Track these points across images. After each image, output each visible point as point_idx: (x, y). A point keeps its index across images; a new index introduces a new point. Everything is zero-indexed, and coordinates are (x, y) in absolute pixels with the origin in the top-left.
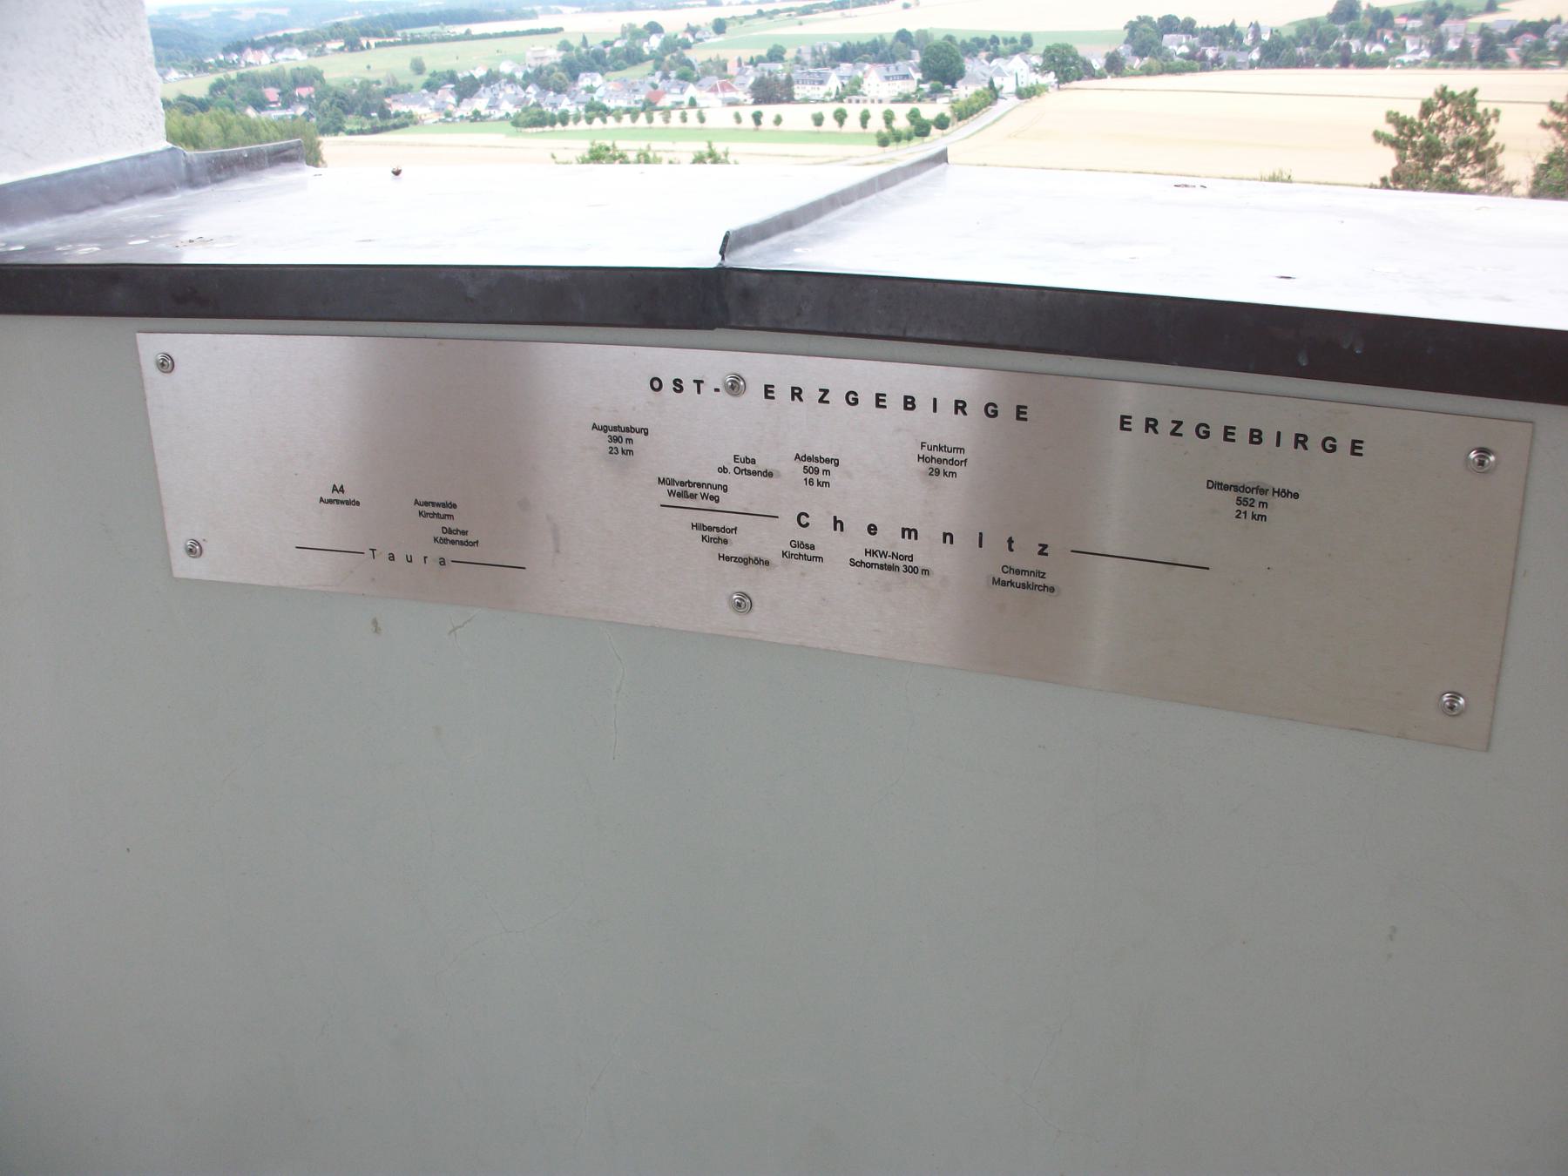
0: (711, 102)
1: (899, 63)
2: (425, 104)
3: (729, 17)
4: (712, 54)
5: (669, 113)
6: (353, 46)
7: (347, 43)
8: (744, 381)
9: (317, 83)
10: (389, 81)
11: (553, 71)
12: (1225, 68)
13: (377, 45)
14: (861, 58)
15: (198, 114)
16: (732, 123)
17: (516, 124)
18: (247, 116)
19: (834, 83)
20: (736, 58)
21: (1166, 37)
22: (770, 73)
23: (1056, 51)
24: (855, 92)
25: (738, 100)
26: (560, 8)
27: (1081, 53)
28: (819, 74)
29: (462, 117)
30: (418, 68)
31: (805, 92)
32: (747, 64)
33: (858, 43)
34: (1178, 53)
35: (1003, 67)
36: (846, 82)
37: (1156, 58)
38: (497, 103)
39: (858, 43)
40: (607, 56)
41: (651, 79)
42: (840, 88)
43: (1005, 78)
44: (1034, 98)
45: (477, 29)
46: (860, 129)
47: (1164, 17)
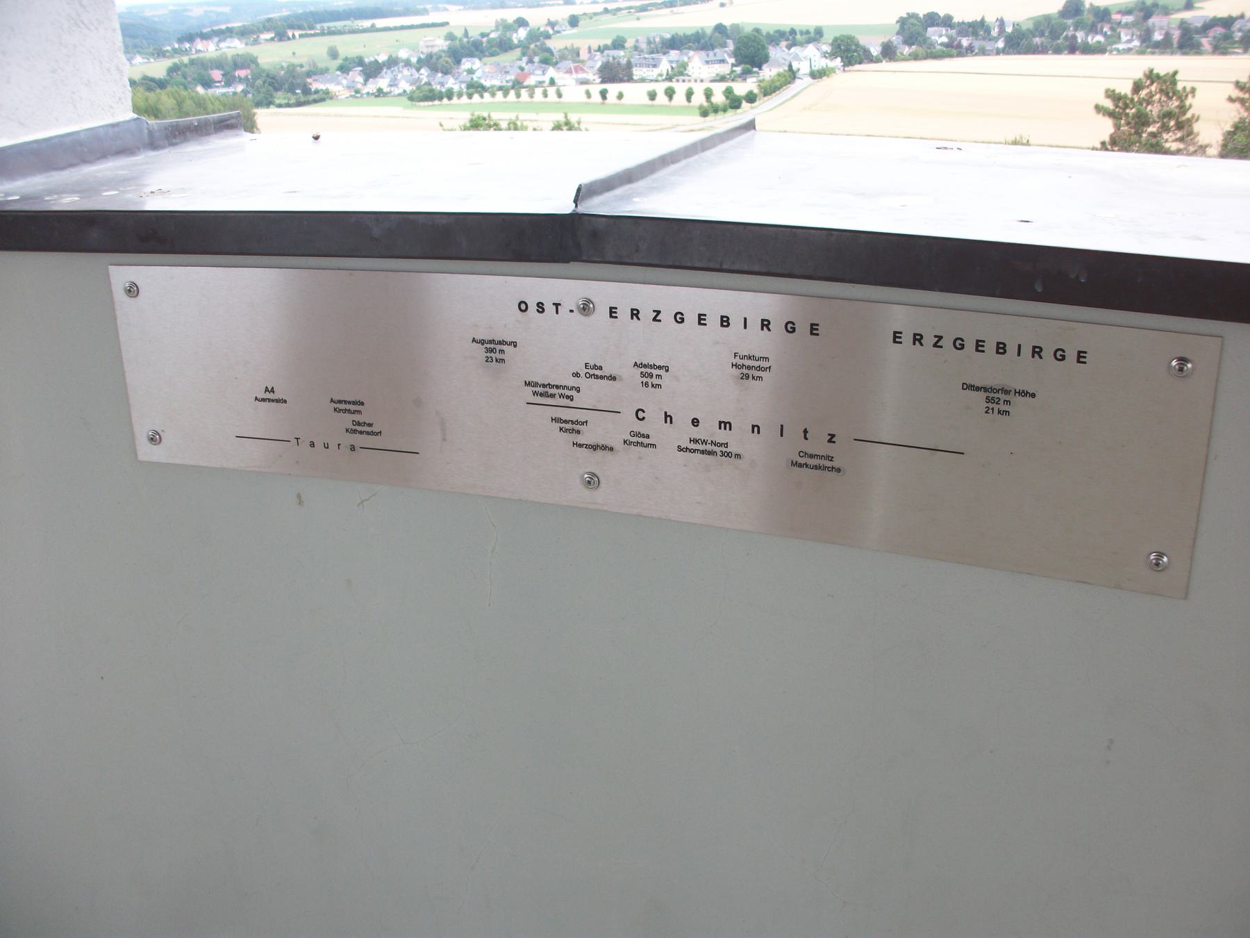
0: (567, 81)
1: (717, 50)
2: (339, 83)
3: (581, 13)
4: (568, 43)
5: (534, 90)
6: (281, 36)
7: (277, 34)
8: (593, 304)
9: (253, 66)
10: (310, 65)
11: (441, 57)
12: (976, 54)
13: (301, 36)
14: (686, 46)
15: (158, 91)
16: (584, 98)
17: (411, 99)
18: (197, 93)
19: (665, 66)
20: (587, 47)
21: (930, 29)
22: (614, 58)
23: (842, 41)
24: (681, 74)
25: (588, 80)
26: (447, 6)
27: (862, 43)
28: (653, 59)
29: (368, 93)
30: (333, 54)
31: (642, 73)
32: (596, 51)
33: (684, 34)
34: (939, 42)
35: (800, 54)
36: (674, 65)
37: (921, 46)
38: (396, 82)
39: (684, 34)
40: (484, 45)
41: (519, 63)
42: (670, 70)
43: (801, 63)
44: (825, 78)
45: (380, 23)
46: (686, 103)
47: (928, 14)
